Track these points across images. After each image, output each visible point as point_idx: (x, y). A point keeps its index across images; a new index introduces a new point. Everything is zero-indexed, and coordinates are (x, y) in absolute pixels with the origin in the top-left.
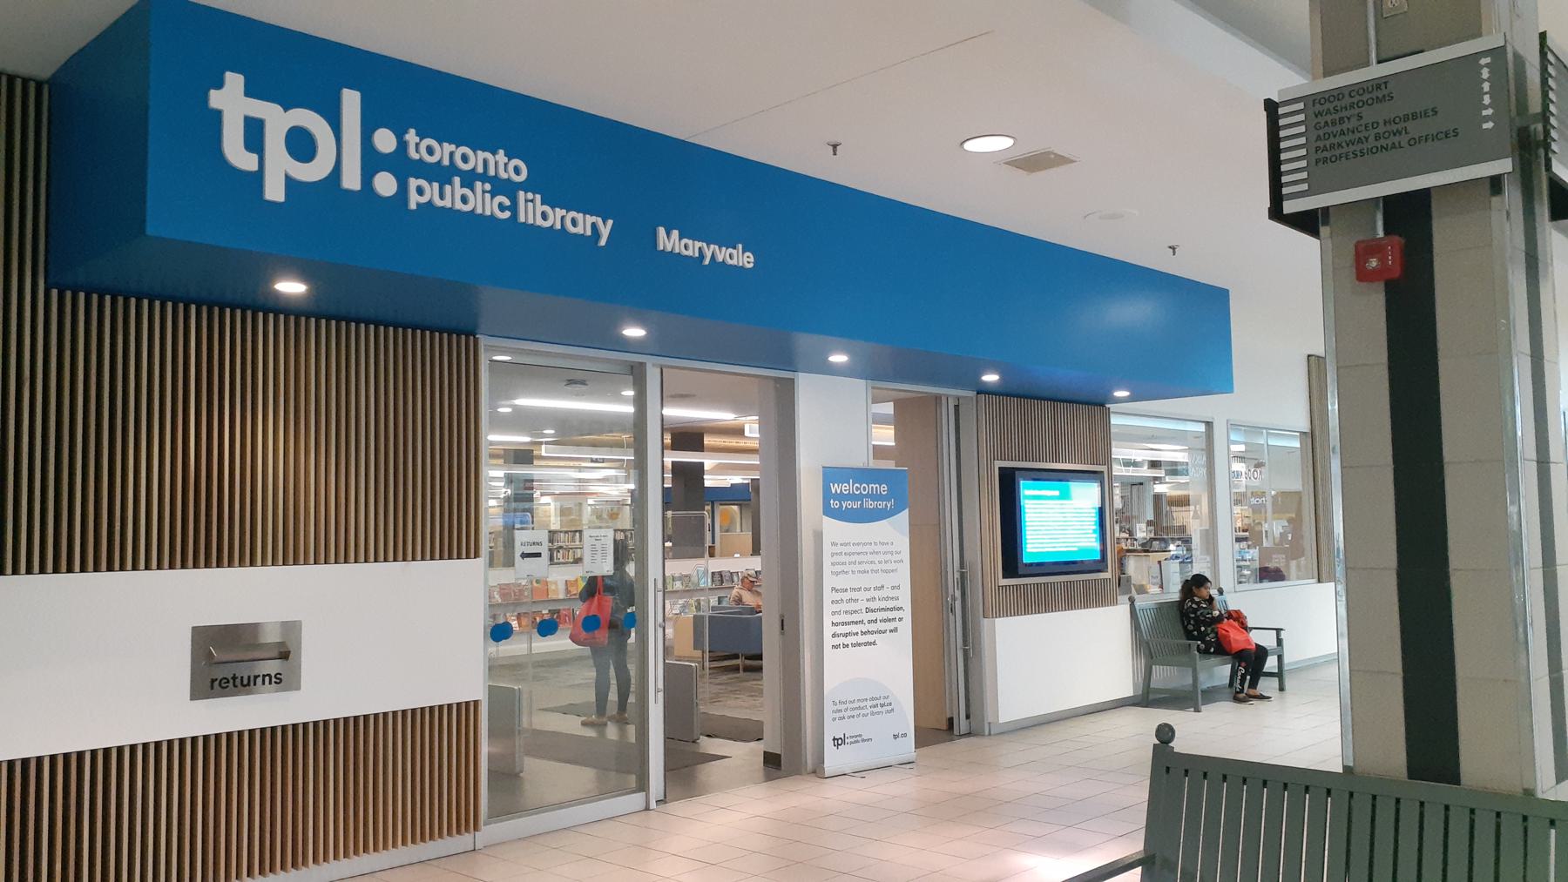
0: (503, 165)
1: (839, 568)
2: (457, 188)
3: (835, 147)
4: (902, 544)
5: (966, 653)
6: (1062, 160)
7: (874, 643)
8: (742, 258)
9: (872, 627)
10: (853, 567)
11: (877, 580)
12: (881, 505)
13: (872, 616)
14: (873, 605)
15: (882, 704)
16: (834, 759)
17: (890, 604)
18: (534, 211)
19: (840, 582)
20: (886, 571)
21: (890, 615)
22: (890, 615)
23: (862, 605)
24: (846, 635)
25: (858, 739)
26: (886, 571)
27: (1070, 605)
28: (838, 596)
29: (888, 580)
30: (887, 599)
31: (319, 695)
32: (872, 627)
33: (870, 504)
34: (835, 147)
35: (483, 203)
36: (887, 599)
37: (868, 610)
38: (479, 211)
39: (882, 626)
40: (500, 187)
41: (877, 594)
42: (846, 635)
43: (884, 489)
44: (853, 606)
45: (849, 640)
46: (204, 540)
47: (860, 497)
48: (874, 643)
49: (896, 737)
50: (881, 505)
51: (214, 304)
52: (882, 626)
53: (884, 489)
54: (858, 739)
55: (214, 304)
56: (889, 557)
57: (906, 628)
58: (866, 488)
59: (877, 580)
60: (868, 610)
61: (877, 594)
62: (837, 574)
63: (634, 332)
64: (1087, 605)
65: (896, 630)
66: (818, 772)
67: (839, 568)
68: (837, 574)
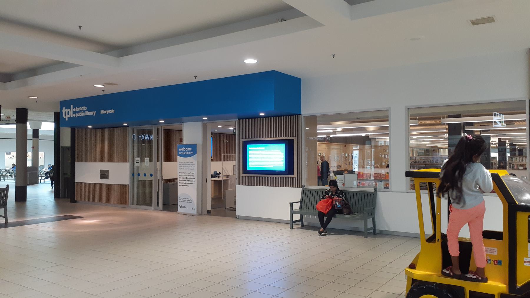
0: (85, 108)
3: (334, 56)
4: (195, 163)
5: (159, 188)
6: (321, 25)
11: (187, 171)
12: (190, 153)
15: (190, 201)
17: (192, 177)
18: (88, 113)
19: (181, 171)
23: (185, 177)
25: (184, 207)
29: (192, 171)
31: (111, 180)
33: (187, 153)
34: (334, 56)
35: (82, 114)
39: (190, 182)
40: (84, 111)
43: (191, 149)
44: (183, 177)
45: (183, 184)
46: (102, 160)
47: (185, 151)
50: (190, 153)
52: (190, 182)
53: (191, 149)
54: (184, 207)
57: (195, 183)
58: (187, 149)
59: (187, 171)
64: (288, 186)
66: (176, 210)
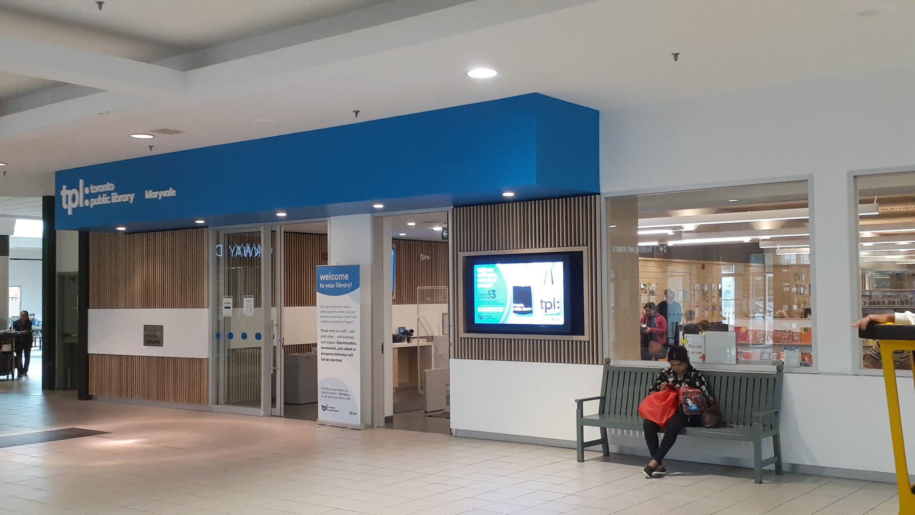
0: (109, 187)
1: (324, 319)
2: (100, 198)
5: (275, 365)
7: (340, 361)
8: (171, 193)
9: (340, 352)
10: (330, 319)
12: (345, 285)
13: (340, 346)
14: (341, 340)
15: (344, 394)
16: (322, 415)
17: (349, 340)
19: (326, 326)
20: (347, 322)
21: (350, 346)
22: (350, 346)
23: (335, 340)
24: (328, 354)
25: (333, 409)
26: (347, 322)
27: (557, 358)
28: (324, 334)
29: (349, 327)
30: (347, 337)
32: (340, 352)
33: (339, 285)
35: (104, 200)
36: (347, 337)
37: (338, 343)
38: (81, 205)
40: (109, 194)
41: (343, 334)
42: (328, 354)
43: (346, 277)
45: (329, 357)
46: (147, 303)
48: (340, 361)
49: (351, 413)
50: (345, 285)
51: (587, 195)
53: (346, 277)
54: (333, 409)
55: (587, 195)
56: (348, 314)
57: (357, 354)
60: (338, 343)
61: (343, 334)
62: (323, 322)
63: (282, 214)
65: (351, 355)
66: (313, 417)
67: (324, 319)
68: (323, 322)
